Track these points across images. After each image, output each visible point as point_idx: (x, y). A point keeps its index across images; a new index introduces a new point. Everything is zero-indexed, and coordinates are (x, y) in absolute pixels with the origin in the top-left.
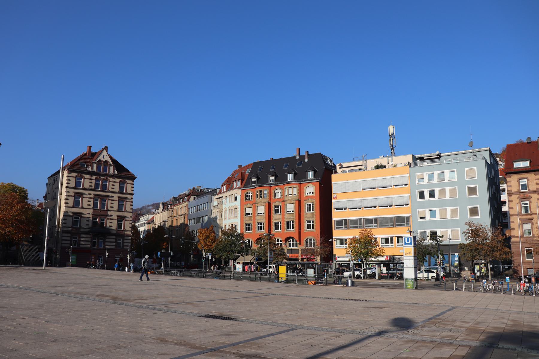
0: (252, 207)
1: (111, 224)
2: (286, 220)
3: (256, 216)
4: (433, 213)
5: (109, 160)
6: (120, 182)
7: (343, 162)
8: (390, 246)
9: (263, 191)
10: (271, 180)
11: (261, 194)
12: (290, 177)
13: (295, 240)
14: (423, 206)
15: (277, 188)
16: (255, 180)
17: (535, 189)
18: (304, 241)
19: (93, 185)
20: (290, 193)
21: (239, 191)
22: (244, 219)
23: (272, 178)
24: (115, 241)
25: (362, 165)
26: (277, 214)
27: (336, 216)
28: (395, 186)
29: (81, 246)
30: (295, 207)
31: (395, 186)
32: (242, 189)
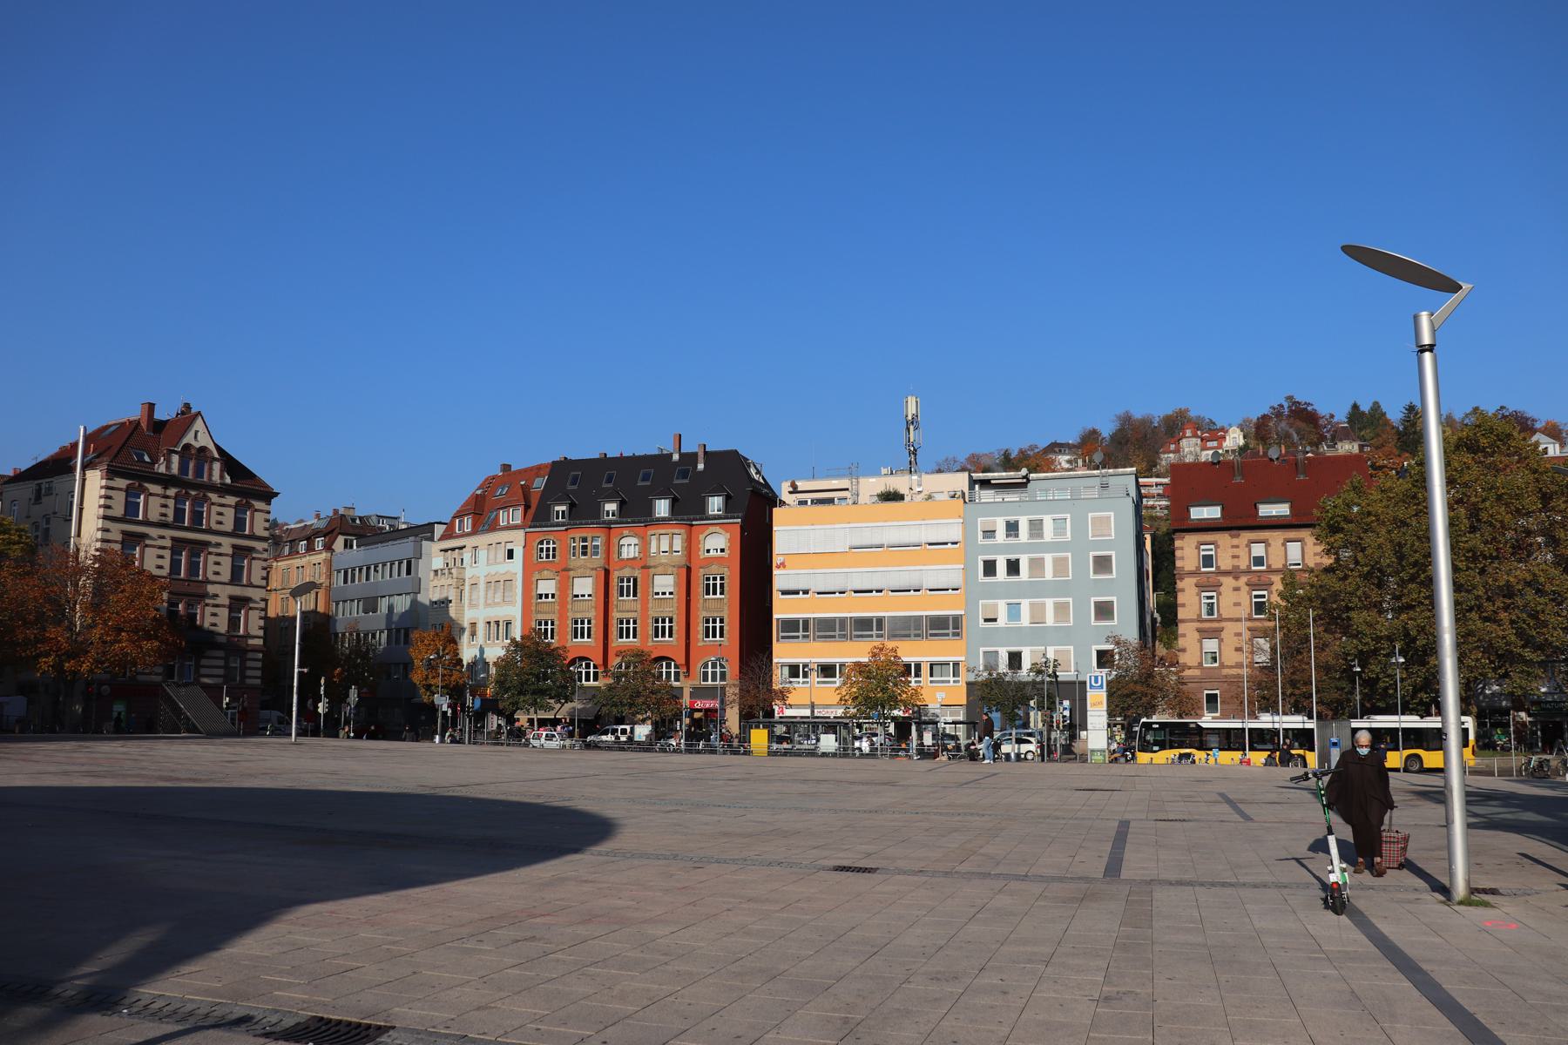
0: (558, 578)
1: (213, 620)
2: (652, 613)
3: (570, 602)
4: (1014, 611)
5: (212, 447)
6: (128, 490)
7: (800, 479)
8: (952, 682)
9: (589, 539)
10: (608, 512)
11: (585, 547)
12: (662, 508)
13: (592, 663)
14: (994, 593)
15: (626, 532)
16: (564, 508)
17: (1230, 568)
18: (697, 668)
19: (170, 512)
20: (664, 547)
21: (520, 535)
22: (533, 608)
23: (611, 507)
24: (248, 662)
25: (847, 489)
26: (625, 598)
27: (782, 609)
28: (930, 544)
29: (249, 681)
30: (677, 584)
31: (930, 544)
32: (528, 530)
